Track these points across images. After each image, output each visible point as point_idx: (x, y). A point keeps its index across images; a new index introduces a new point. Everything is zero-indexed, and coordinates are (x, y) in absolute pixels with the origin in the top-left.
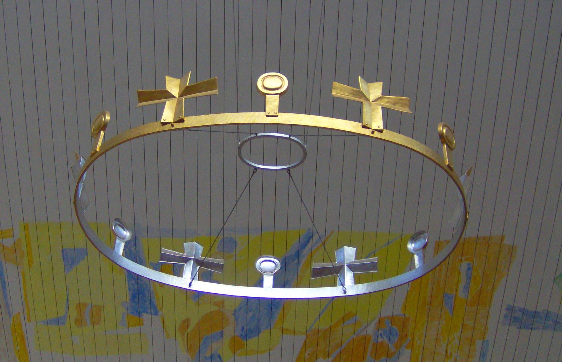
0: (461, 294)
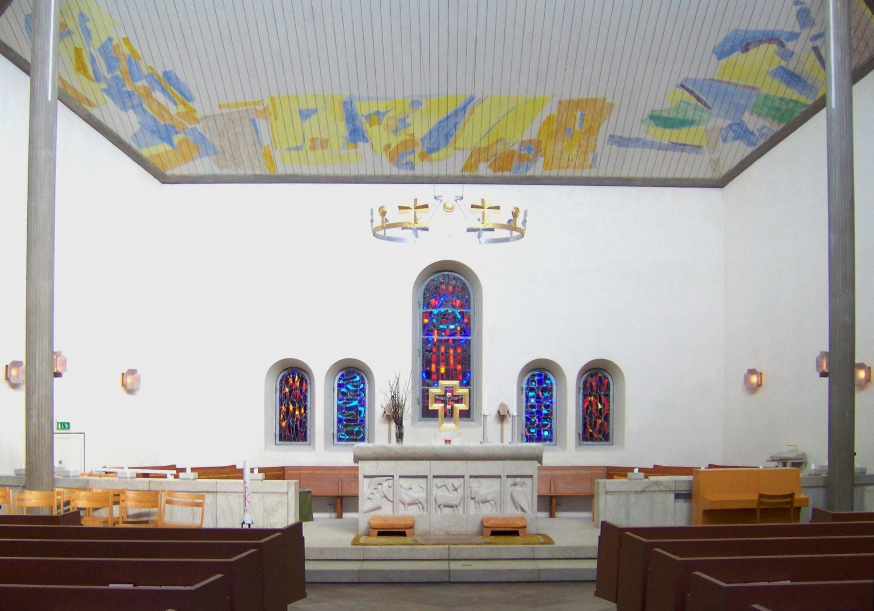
0: (577, 128)
